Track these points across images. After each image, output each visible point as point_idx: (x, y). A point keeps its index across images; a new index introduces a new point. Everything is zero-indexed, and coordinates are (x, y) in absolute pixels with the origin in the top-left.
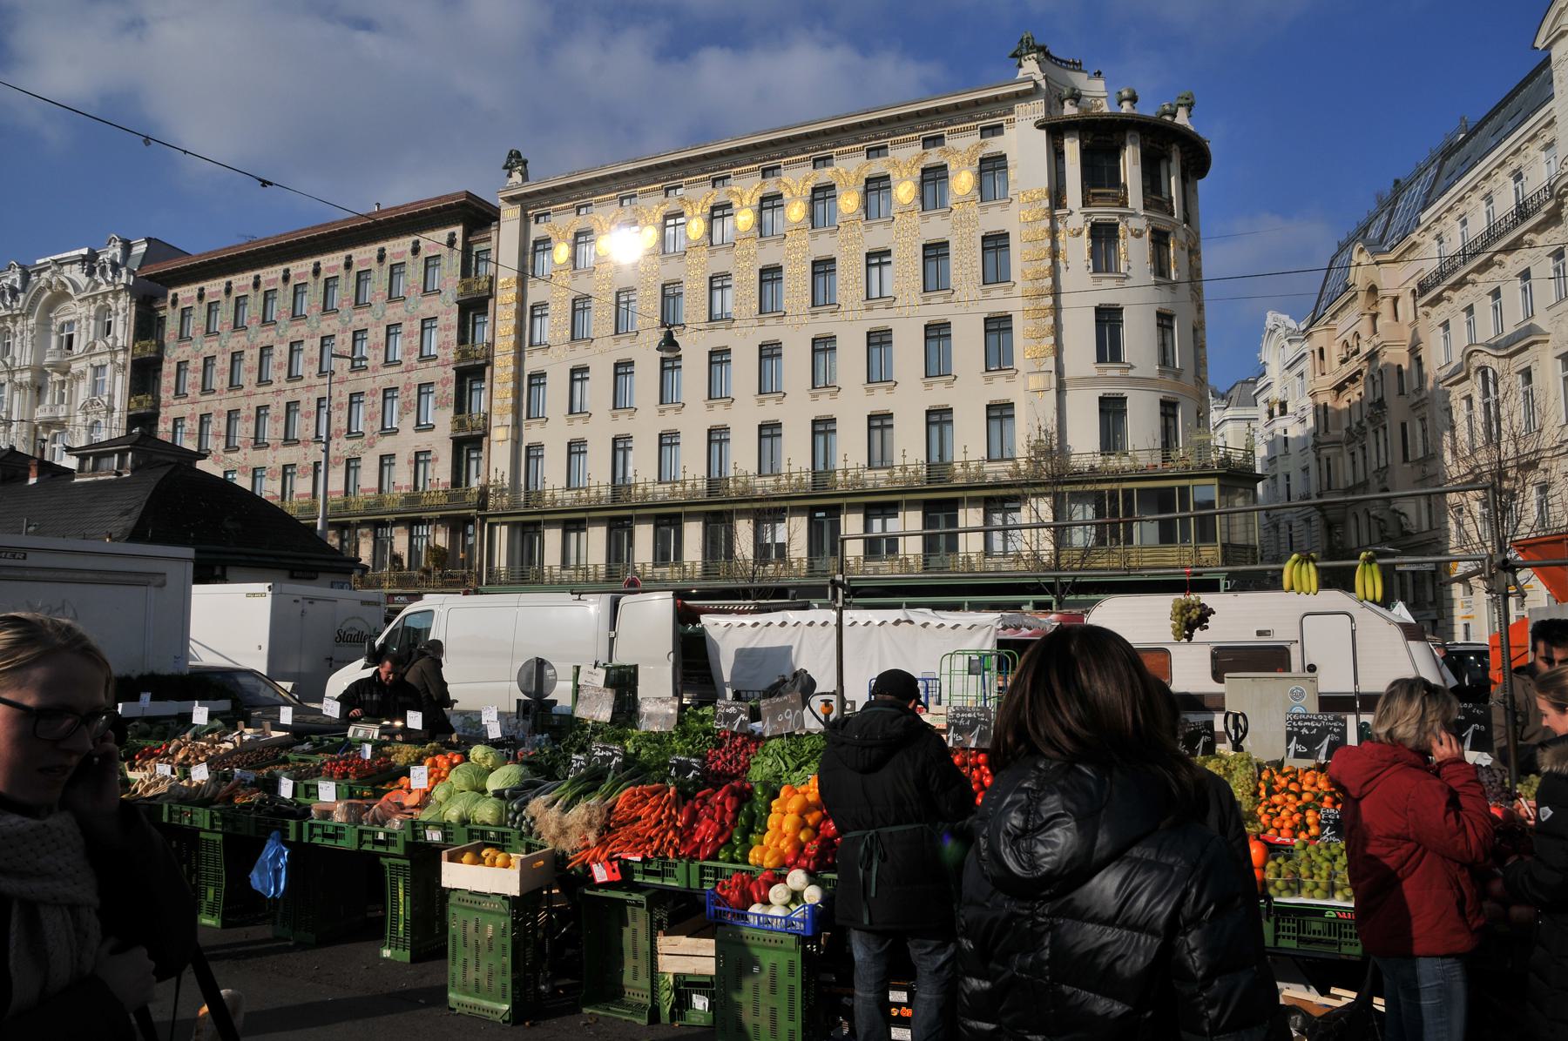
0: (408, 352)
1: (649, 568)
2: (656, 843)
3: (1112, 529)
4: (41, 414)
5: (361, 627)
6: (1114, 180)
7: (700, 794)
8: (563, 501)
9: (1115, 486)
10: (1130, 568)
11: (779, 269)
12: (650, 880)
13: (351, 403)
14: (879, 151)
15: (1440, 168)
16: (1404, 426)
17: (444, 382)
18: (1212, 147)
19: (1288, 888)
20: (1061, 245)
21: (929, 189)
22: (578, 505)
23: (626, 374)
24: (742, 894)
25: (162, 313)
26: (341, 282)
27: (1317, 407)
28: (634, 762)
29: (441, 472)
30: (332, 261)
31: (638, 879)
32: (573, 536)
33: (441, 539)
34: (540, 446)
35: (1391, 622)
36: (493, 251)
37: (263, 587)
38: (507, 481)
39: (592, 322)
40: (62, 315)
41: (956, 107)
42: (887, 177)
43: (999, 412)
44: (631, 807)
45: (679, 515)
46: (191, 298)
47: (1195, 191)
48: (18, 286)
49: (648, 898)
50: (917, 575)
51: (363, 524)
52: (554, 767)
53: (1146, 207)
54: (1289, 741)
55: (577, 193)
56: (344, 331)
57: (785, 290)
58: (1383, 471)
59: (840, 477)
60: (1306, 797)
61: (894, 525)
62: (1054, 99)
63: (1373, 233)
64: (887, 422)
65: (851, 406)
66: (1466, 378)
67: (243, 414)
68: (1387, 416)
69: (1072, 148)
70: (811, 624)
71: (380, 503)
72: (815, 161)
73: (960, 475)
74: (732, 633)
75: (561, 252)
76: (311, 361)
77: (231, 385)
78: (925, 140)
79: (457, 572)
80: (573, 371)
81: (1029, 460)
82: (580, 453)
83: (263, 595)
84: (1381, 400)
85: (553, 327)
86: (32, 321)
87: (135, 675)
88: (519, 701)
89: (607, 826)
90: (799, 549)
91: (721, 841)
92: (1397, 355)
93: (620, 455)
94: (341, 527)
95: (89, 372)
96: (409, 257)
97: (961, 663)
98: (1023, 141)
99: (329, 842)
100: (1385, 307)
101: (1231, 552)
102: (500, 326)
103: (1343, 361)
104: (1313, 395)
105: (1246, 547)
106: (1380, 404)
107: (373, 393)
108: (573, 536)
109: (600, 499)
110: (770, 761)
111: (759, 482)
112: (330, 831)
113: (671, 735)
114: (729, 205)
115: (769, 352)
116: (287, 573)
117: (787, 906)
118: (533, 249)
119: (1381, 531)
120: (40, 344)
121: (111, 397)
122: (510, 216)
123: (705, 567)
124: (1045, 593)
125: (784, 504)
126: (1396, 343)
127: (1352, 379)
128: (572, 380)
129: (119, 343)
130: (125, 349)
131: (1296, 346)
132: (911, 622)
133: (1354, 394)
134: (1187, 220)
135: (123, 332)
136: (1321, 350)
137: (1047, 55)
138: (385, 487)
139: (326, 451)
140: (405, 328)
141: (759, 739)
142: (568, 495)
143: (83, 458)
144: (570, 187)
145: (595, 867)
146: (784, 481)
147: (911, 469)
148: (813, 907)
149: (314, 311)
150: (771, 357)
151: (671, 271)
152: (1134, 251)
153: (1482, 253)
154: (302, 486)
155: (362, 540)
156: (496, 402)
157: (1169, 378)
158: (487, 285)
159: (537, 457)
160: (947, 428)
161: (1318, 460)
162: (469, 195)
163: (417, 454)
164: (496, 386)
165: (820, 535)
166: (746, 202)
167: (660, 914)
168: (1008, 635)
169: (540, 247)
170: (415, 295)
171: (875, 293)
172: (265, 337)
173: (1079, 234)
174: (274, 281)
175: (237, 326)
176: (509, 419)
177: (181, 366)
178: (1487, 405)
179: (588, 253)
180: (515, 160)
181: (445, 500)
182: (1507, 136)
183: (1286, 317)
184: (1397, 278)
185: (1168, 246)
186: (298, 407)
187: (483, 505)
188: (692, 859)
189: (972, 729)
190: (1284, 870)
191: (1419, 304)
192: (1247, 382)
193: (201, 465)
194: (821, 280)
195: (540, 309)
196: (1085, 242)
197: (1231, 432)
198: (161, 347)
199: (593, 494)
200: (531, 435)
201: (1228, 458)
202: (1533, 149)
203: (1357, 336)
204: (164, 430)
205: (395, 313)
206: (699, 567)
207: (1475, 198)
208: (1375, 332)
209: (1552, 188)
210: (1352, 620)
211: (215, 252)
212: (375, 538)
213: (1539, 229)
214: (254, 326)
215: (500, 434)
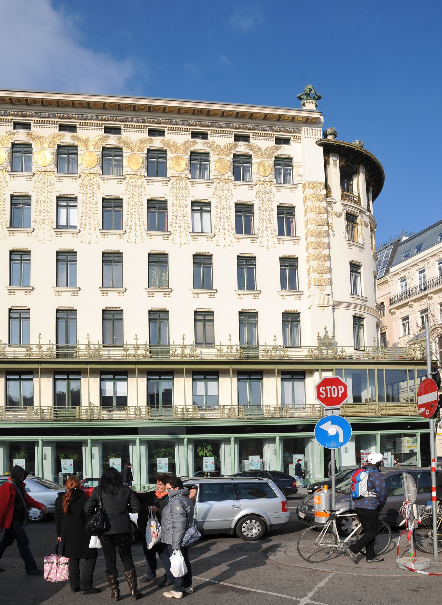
61: (121, 388)
73: (82, 353)
98: (306, 151)
171: (198, 228)
173: (340, 216)
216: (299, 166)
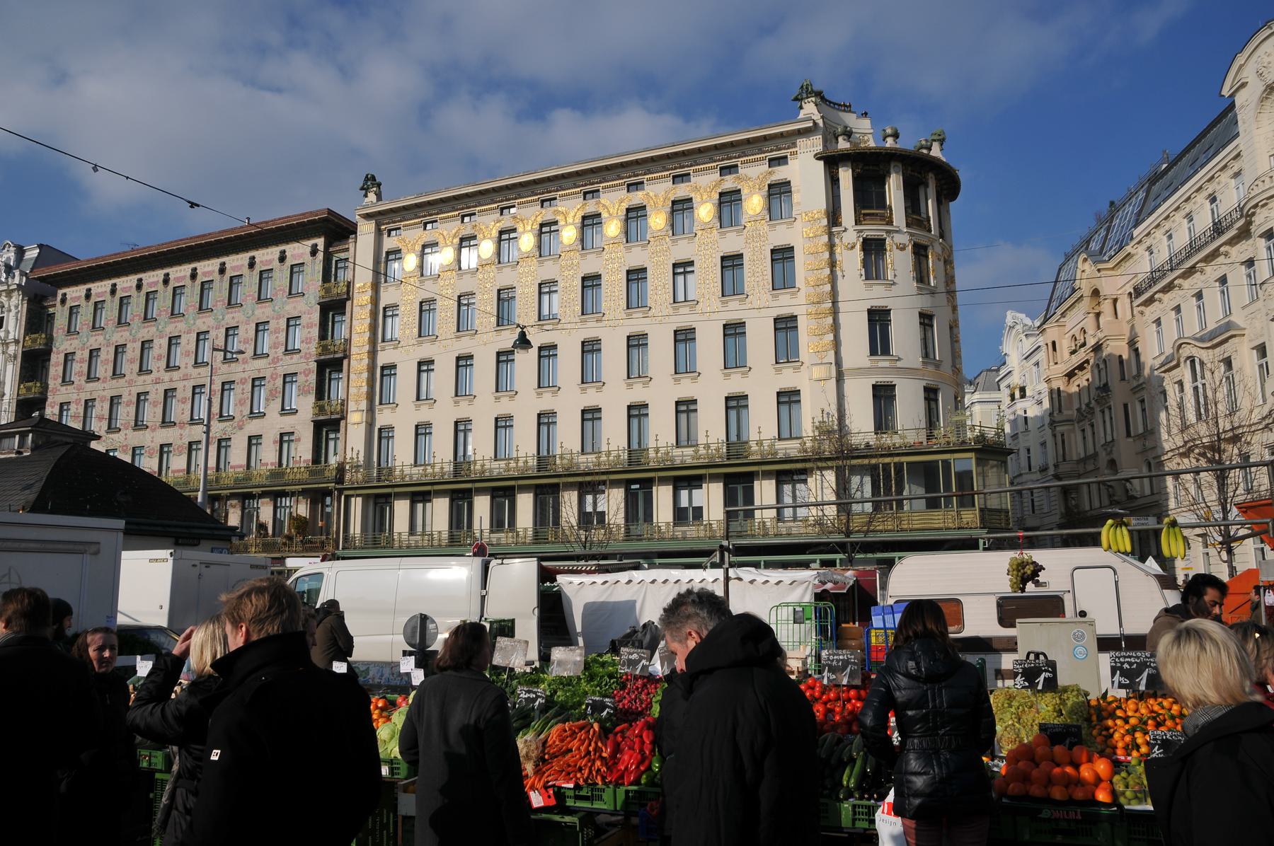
0: (275, 346)
1: (486, 534)
6: (881, 202)
7: (618, 729)
9: (887, 460)
10: (902, 530)
11: (598, 277)
12: (579, 804)
13: (223, 390)
15: (1148, 192)
16: (1126, 406)
19: (1136, 797)
20: (838, 257)
21: (726, 210)
22: (424, 480)
26: (216, 285)
27: (1051, 392)
29: (303, 451)
31: (570, 803)
32: (420, 506)
33: (303, 509)
34: (391, 428)
35: (1148, 574)
37: (165, 553)
38: (361, 458)
39: (437, 322)
41: (748, 141)
42: (690, 200)
43: (788, 398)
44: (562, 741)
45: (513, 488)
47: (948, 211)
50: (619, 546)
51: (233, 496)
53: (908, 225)
54: (1113, 675)
57: (603, 294)
58: (1110, 445)
59: (652, 454)
60: (1133, 721)
62: (830, 135)
63: (1094, 246)
64: (692, 407)
66: (1177, 366)
67: (124, 399)
68: (1113, 397)
69: (845, 176)
70: (653, 582)
72: (629, 186)
74: (582, 590)
75: (410, 262)
76: (187, 354)
78: (721, 169)
79: (317, 538)
80: (420, 364)
82: (426, 434)
83: (165, 560)
84: (1106, 385)
85: (402, 326)
92: (1117, 347)
93: (461, 435)
96: (276, 263)
97: (787, 613)
98: (804, 170)
100: (1106, 307)
101: (990, 518)
103: (1073, 352)
104: (1048, 381)
105: (999, 511)
106: (1105, 388)
107: (243, 382)
108: (420, 506)
109: (443, 474)
111: (582, 459)
113: (579, 679)
114: (556, 223)
115: (590, 348)
116: (172, 540)
118: (383, 260)
119: (1110, 496)
122: (366, 230)
123: (536, 532)
124: (837, 552)
125: (604, 477)
126: (1117, 337)
127: (1081, 367)
128: (419, 371)
129: (11, 336)
130: (17, 342)
131: (1032, 339)
132: (740, 579)
133: (1083, 379)
134: (942, 236)
136: (1054, 343)
137: (823, 99)
138: (253, 464)
139: (207, 433)
140: (272, 326)
142: (415, 470)
146: (604, 458)
147: (713, 447)
149: (191, 310)
150: (592, 351)
152: (899, 261)
153: (1184, 265)
154: (178, 463)
155: (231, 511)
157: (931, 368)
159: (388, 438)
160: (744, 411)
161: (1054, 436)
162: (330, 212)
163: (282, 435)
164: (352, 376)
166: (570, 220)
170: (281, 297)
171: (681, 297)
172: (146, 332)
173: (853, 247)
174: (156, 283)
175: (120, 322)
177: (68, 357)
178: (1196, 389)
180: (371, 183)
181: (306, 476)
182: (1202, 166)
183: (1022, 316)
184: (1116, 283)
185: (927, 257)
188: (617, 785)
189: (844, 668)
190: (1131, 783)
191: (1135, 304)
192: (990, 370)
193: (94, 445)
194: (634, 286)
196: (858, 254)
197: (983, 413)
198: (50, 340)
199: (437, 469)
200: (382, 418)
202: (1225, 177)
203: (1084, 331)
205: (263, 312)
206: (530, 533)
207: (1178, 217)
208: (1099, 328)
209: (1241, 210)
211: (103, 258)
212: (243, 509)
213: (1232, 242)
214: (136, 322)
215: (356, 417)
216: (798, 191)
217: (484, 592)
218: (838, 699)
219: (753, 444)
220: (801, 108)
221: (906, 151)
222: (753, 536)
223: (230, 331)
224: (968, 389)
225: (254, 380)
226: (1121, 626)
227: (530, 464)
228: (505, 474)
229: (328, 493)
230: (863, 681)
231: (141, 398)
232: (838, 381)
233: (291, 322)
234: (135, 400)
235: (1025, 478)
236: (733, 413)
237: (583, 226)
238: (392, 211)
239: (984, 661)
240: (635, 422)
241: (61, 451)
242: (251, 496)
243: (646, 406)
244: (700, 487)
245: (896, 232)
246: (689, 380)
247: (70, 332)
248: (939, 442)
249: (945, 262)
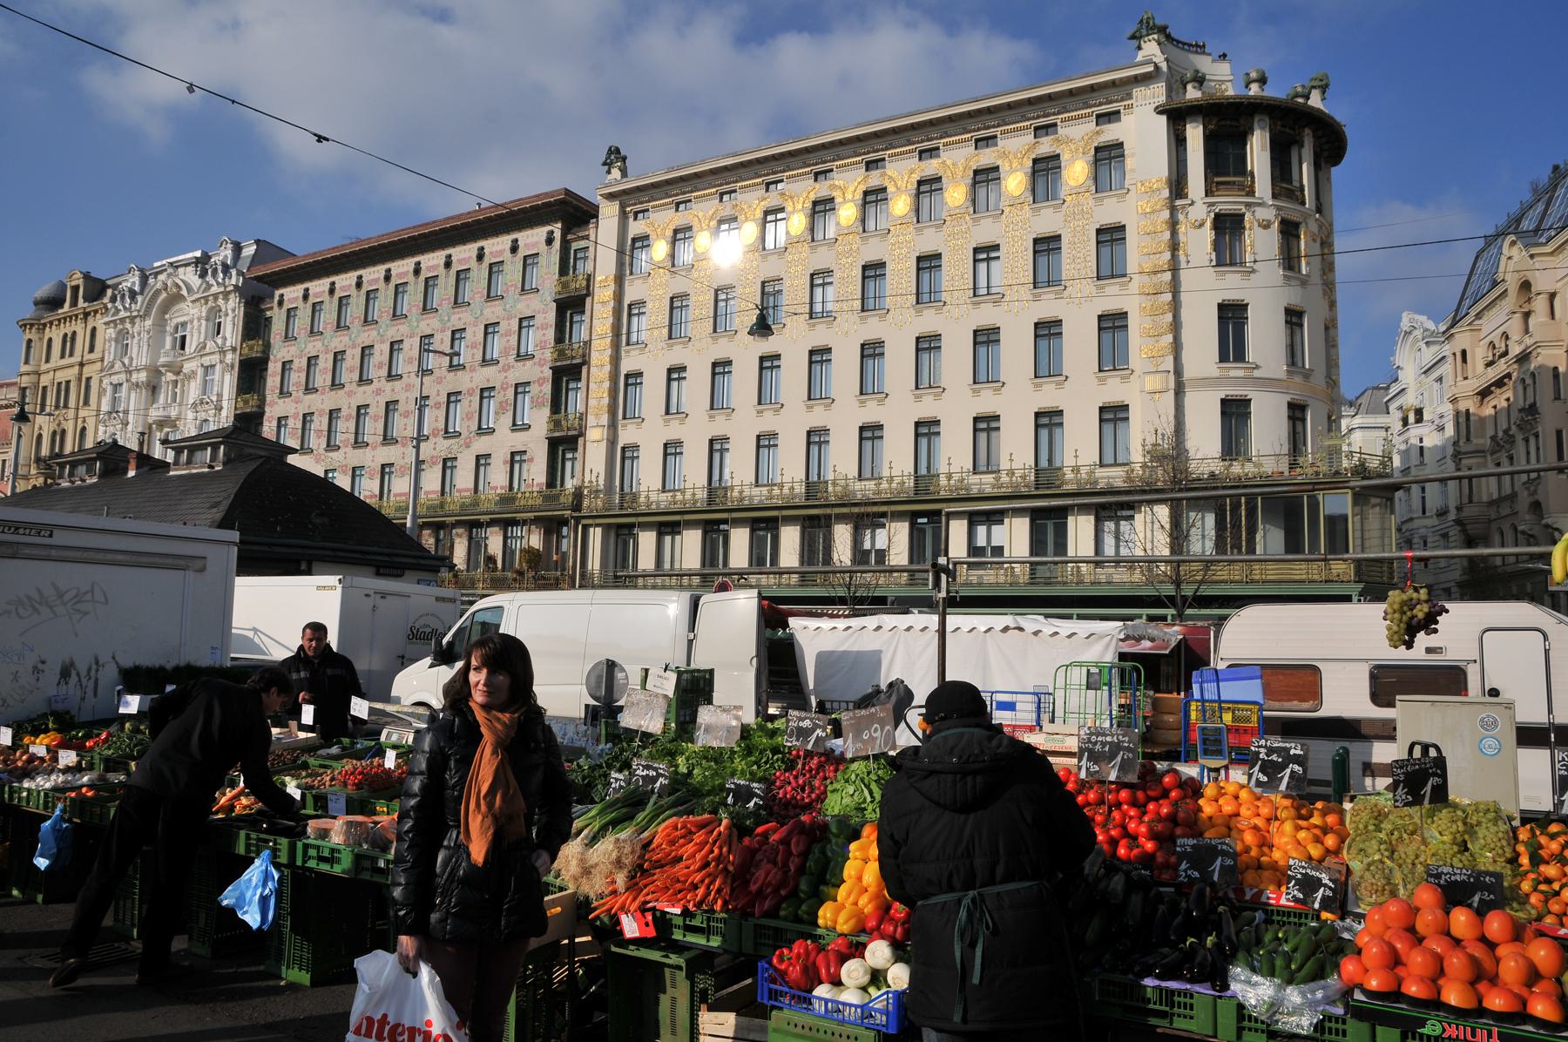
0: (505, 352)
2: (701, 892)
3: (1233, 536)
4: (155, 413)
5: (434, 624)
6: (1240, 167)
7: (760, 830)
8: (658, 503)
10: (1253, 581)
11: (882, 265)
12: (692, 939)
14: (987, 141)
16: (1559, 433)
17: (541, 381)
18: (1349, 132)
20: (1182, 238)
22: (673, 508)
23: (724, 373)
24: (805, 969)
25: (268, 314)
26: (441, 281)
27: (1457, 414)
28: (685, 783)
29: (536, 472)
30: (432, 261)
31: (678, 935)
32: (668, 539)
33: (535, 540)
34: (636, 447)
36: (592, 249)
37: (332, 580)
38: (601, 481)
40: (176, 317)
42: (997, 169)
43: (1114, 415)
44: (672, 843)
46: (296, 299)
47: (1329, 179)
48: (137, 288)
49: (688, 962)
52: (591, 786)
53: (1274, 196)
55: (678, 188)
56: (443, 331)
57: (888, 287)
59: (943, 481)
62: (1176, 82)
63: (1526, 225)
64: (994, 425)
65: (956, 411)
67: (344, 413)
69: (1195, 134)
71: (476, 503)
72: (921, 152)
73: (1070, 480)
74: (815, 636)
75: (660, 250)
76: (410, 361)
77: (333, 384)
78: (1036, 129)
79: (543, 572)
80: (670, 371)
81: (1144, 466)
83: (333, 588)
85: (652, 324)
86: (149, 323)
87: (169, 666)
88: (587, 706)
89: (640, 866)
90: (899, 555)
91: (783, 892)
93: (717, 456)
94: (437, 527)
95: (200, 372)
96: (507, 255)
97: (1078, 676)
98: (1142, 127)
99: (325, 867)
100: (1540, 305)
102: (598, 322)
104: (1454, 401)
107: (470, 392)
108: (668, 539)
109: (696, 502)
110: (851, 789)
111: (858, 486)
112: (326, 854)
113: (733, 752)
116: (373, 570)
117: (864, 989)
118: (630, 248)
120: (155, 345)
121: (220, 395)
122: (609, 213)
124: (1165, 606)
127: (1500, 383)
128: (669, 380)
130: (234, 349)
131: (1434, 348)
132: (1021, 629)
133: (1500, 399)
134: (1319, 210)
135: (232, 332)
136: (1464, 353)
137: (1168, 37)
138: (481, 487)
140: (502, 328)
141: (838, 761)
142: (663, 497)
143: (179, 451)
144: (668, 182)
145: (623, 917)
146: (885, 485)
147: (1018, 473)
148: (899, 995)
149: (414, 310)
150: (874, 356)
151: (769, 270)
152: (1261, 242)
154: (401, 485)
155: (457, 541)
156: (592, 402)
157: (1298, 379)
158: (584, 283)
159: (633, 458)
160: (1057, 431)
162: (567, 192)
163: (513, 454)
165: (922, 540)
166: (849, 196)
167: (704, 981)
168: (1127, 648)
169: (638, 244)
173: (1201, 225)
174: (376, 281)
175: (340, 326)
176: (605, 420)
177: (286, 366)
179: (685, 255)
180: (615, 157)
181: (539, 501)
183: (1423, 318)
185: (1298, 237)
186: (400, 409)
187: (577, 507)
189: (1112, 756)
192: (1378, 388)
194: (925, 276)
195: (637, 307)
196: (1208, 234)
197: (1363, 438)
198: (267, 347)
199: (688, 496)
200: (626, 435)
201: (1362, 463)
203: (1506, 336)
204: (268, 430)
205: (492, 312)
208: (1527, 331)
210: (1546, 638)
211: (320, 253)
212: (470, 538)
214: (356, 325)
215: (595, 435)
216: (1133, 155)
217: (691, 636)
218: (1101, 802)
219: (1067, 471)
220: (1139, 48)
221: (1275, 99)
222: (1065, 583)
223: (457, 334)
224: (1346, 411)
225: (482, 390)
226: (1550, 711)
227: (797, 491)
228: (768, 503)
229: (563, 522)
230: (1142, 777)
231: (361, 411)
232: (1177, 394)
233: (524, 322)
234: (354, 414)
235: (1416, 524)
236: (1044, 433)
237: (865, 203)
238: (638, 189)
239: (1346, 751)
240: (924, 442)
241: (252, 466)
242: (477, 524)
243: (937, 423)
244: (1001, 522)
245: (1259, 205)
246: (990, 392)
247: (288, 337)
248: (1305, 473)
249: (1323, 244)
